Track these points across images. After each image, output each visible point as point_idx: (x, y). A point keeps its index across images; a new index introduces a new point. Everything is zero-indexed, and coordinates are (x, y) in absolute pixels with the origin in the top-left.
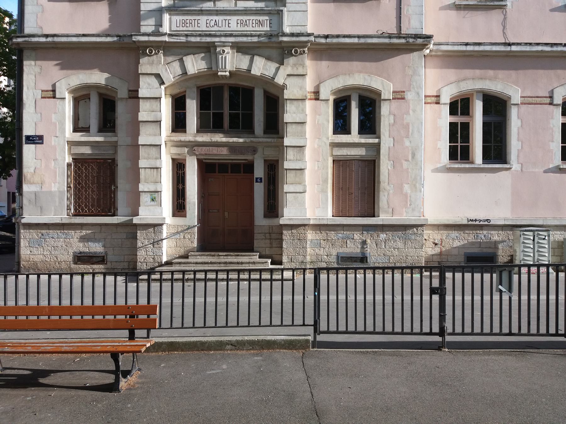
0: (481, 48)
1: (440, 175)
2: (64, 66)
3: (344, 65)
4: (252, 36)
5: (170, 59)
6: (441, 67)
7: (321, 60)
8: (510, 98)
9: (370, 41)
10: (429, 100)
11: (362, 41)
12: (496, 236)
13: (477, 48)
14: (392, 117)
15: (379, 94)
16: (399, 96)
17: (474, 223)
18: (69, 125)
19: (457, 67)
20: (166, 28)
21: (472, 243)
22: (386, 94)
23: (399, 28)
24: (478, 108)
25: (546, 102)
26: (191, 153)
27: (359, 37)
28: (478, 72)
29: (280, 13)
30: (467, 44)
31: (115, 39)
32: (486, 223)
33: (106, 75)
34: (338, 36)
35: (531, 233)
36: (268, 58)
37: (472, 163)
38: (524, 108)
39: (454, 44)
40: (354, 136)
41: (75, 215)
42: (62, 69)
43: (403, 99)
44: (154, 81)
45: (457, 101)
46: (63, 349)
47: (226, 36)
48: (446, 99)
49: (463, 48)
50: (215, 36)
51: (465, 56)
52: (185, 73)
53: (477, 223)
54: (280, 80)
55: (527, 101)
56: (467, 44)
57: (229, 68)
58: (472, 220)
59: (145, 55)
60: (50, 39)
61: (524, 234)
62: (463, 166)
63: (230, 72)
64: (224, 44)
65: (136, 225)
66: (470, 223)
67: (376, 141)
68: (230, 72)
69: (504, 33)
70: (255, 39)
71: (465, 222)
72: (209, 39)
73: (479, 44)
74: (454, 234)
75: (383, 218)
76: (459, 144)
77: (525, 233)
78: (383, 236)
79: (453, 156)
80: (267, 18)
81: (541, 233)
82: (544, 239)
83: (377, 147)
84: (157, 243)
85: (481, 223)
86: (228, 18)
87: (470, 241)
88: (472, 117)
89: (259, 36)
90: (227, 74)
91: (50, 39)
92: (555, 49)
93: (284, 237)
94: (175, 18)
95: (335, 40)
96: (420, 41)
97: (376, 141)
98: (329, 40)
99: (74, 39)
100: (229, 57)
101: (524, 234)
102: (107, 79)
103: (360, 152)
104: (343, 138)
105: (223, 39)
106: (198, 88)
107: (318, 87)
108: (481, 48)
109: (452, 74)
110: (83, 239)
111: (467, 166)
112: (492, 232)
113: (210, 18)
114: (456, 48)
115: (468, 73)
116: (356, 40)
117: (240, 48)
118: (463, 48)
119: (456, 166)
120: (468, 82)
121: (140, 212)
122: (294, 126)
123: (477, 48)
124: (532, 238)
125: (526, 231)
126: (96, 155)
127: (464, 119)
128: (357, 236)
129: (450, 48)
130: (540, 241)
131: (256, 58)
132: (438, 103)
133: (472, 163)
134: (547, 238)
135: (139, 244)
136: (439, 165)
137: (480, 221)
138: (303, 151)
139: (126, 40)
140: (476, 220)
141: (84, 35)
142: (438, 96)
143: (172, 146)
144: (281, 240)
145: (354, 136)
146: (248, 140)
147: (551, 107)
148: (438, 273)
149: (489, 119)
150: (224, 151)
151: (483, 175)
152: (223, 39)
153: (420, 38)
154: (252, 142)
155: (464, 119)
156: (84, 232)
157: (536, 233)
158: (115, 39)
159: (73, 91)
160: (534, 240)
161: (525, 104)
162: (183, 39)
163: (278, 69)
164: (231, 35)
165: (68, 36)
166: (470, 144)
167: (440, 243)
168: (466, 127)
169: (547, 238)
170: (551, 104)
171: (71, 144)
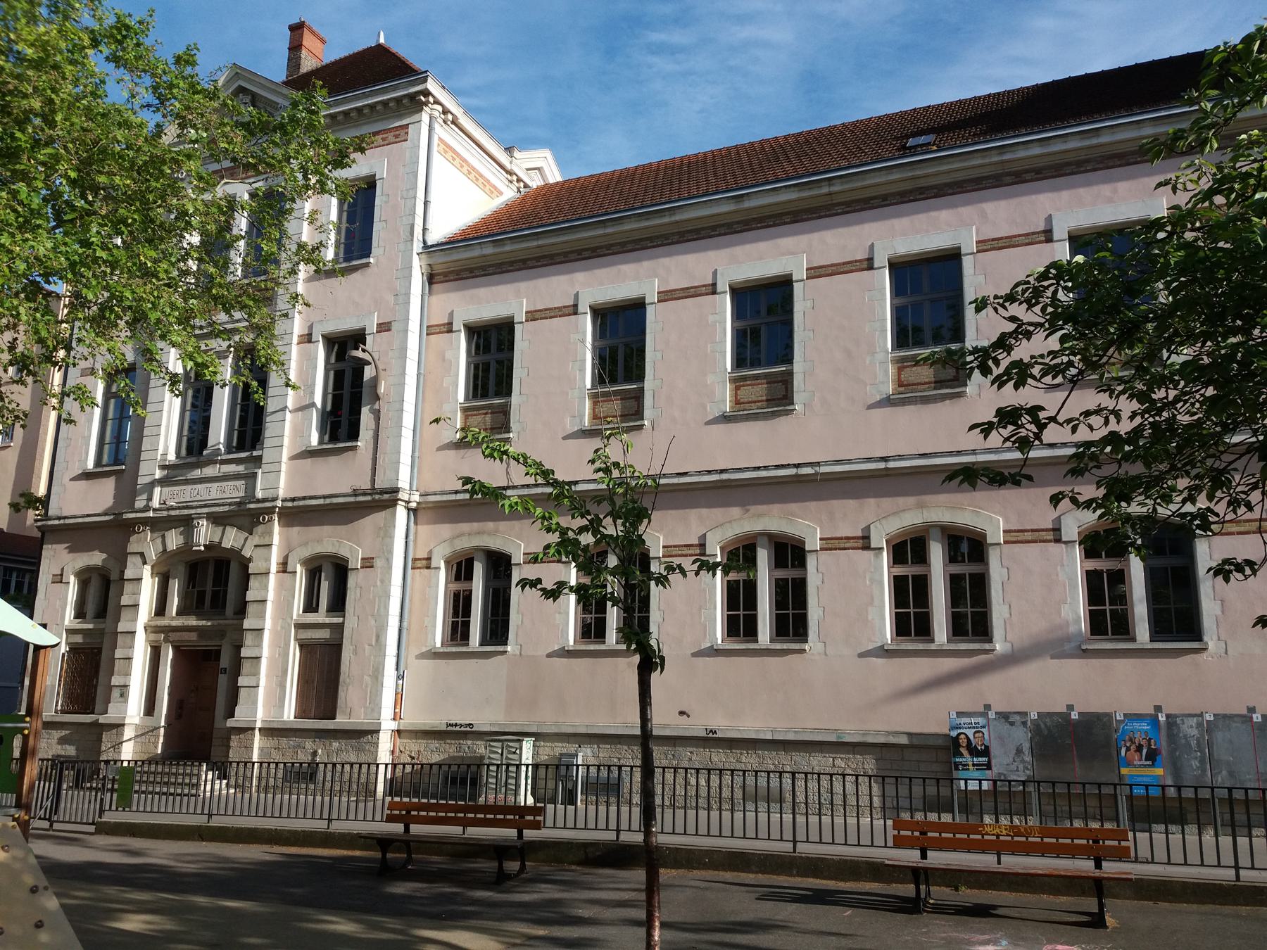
1: (426, 662)
2: (72, 550)
3: (315, 531)
4: (223, 505)
5: (156, 535)
7: (292, 526)
8: (984, 536)
9: (335, 501)
10: (419, 564)
11: (328, 501)
12: (481, 748)
14: (358, 590)
16: (368, 563)
17: (454, 729)
18: (70, 612)
20: (156, 503)
21: (454, 758)
22: (355, 562)
23: (373, 481)
25: (1049, 538)
26: (166, 640)
27: (325, 497)
28: (475, 526)
29: (254, 476)
31: (112, 517)
32: (468, 729)
33: (104, 556)
34: (304, 498)
35: (499, 744)
36: (240, 528)
38: (825, 555)
39: (443, 493)
40: (321, 617)
41: (63, 712)
42: (69, 552)
43: (372, 567)
44: (138, 559)
45: (738, 549)
46: (1037, 918)
47: (201, 507)
48: (879, 539)
50: (192, 508)
51: (454, 506)
52: (165, 550)
54: (247, 553)
55: (1015, 537)
57: (202, 542)
58: (451, 725)
59: (134, 532)
60: (62, 522)
61: (490, 746)
63: (205, 546)
64: (200, 516)
65: (102, 725)
66: (450, 728)
67: (341, 620)
68: (205, 546)
69: (507, 473)
70: (226, 508)
71: (444, 728)
72: (186, 512)
73: (685, 474)
74: (434, 744)
75: (341, 721)
77: (492, 744)
78: (336, 744)
79: (902, 627)
80: (243, 482)
81: (511, 744)
82: (514, 753)
83: (340, 627)
84: (118, 745)
85: (463, 729)
86: (210, 485)
87: (451, 755)
89: (230, 504)
90: (202, 548)
91: (62, 522)
93: (232, 744)
94: (167, 490)
95: (301, 503)
96: (386, 496)
97: (341, 620)
98: (296, 503)
99: (80, 520)
100: (203, 530)
101: (490, 746)
102: (104, 560)
103: (324, 634)
104: (311, 618)
105: (199, 511)
106: (186, 563)
107: (286, 558)
109: (446, 530)
110: (62, 741)
112: (478, 742)
113: (195, 486)
114: (445, 498)
115: (465, 527)
116: (321, 501)
117: (217, 520)
118: (882, 465)
120: (463, 538)
121: (109, 710)
122: (255, 605)
124: (500, 751)
125: (492, 741)
126: (88, 644)
128: (309, 744)
129: (438, 498)
130: (510, 756)
131: (228, 529)
132: (428, 567)
134: (518, 752)
135: (103, 748)
136: (424, 650)
137: (461, 726)
138: (262, 634)
139: (242, 508)
140: (456, 725)
141: (88, 516)
142: (429, 559)
143: (152, 632)
144: (228, 747)
145: (321, 617)
146: (216, 622)
147: (866, 553)
150: (193, 636)
152: (199, 511)
153: (386, 493)
154: (219, 625)
156: (64, 733)
157: (506, 743)
158: (112, 517)
159: (306, 562)
160: (502, 754)
161: (826, 549)
162: (792, 471)
163: (246, 539)
164: (205, 506)
166: (726, 613)
167: (416, 756)
168: (751, 587)
169: (518, 752)
170: (1058, 540)
171: (300, 626)
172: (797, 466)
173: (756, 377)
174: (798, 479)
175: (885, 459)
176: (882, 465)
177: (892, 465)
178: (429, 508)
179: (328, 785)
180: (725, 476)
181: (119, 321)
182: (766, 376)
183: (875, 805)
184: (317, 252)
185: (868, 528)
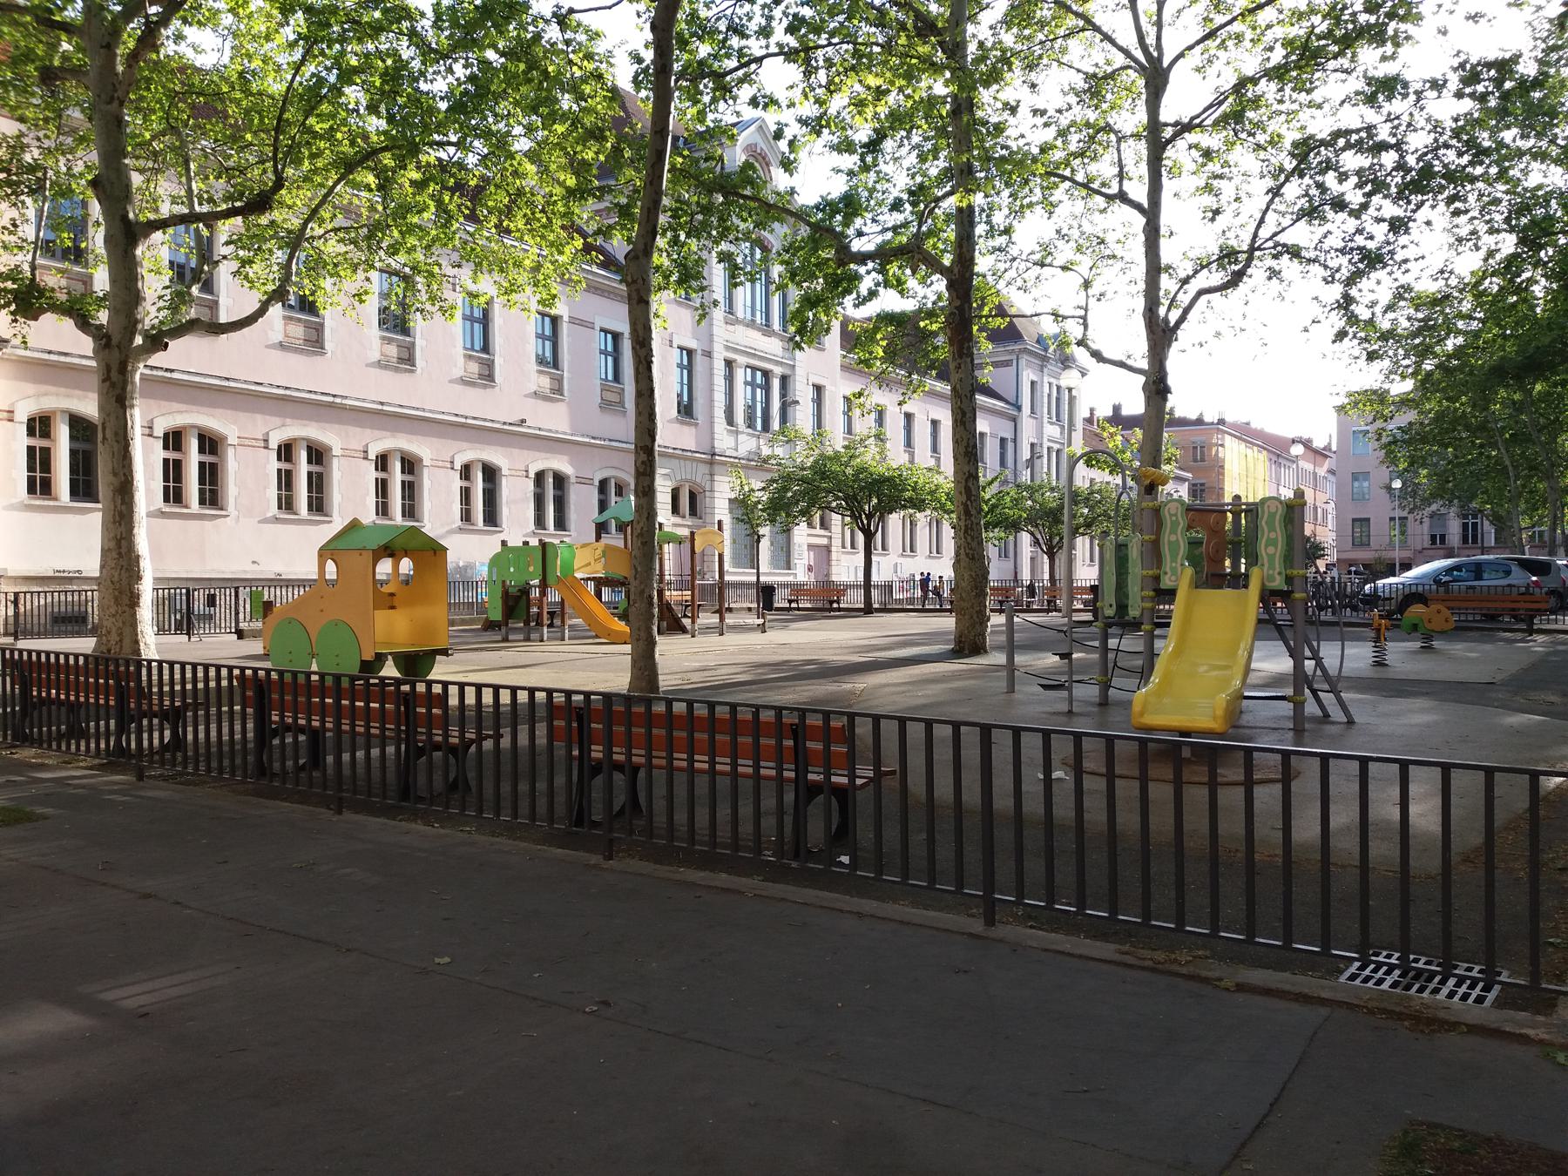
0: (68, 360)
6: (16, 378)
13: (62, 359)
15: (223, 438)
19: (36, 381)
24: (62, 433)
30: (50, 352)
37: (56, 499)
48: (22, 416)
49: (46, 356)
51: (27, 362)
53: (66, 574)
56: (50, 352)
62: (318, 518)
71: (51, 574)
73: (66, 354)
76: (38, 474)
79: (31, 489)
88: (54, 441)
92: (155, 373)
108: (68, 360)
109: (30, 388)
111: (51, 503)
118: (46, 356)
119: (38, 502)
123: (62, 359)
127: (44, 443)
132: (11, 420)
133: (56, 499)
136: (14, 501)
148: (953, 620)
149: (79, 446)
151: (70, 516)
155: (44, 443)
162: (330, 399)
165: (485, 420)
166: (184, 485)
168: (178, 464)
172: (334, 396)
173: (299, 320)
174: (331, 405)
175: (382, 404)
176: (380, 407)
177: (385, 408)
178: (11, 360)
179: (945, 853)
180: (288, 392)
181: (1389, 44)
182: (306, 321)
183: (1088, 765)
184: (753, 66)
185: (268, 433)
